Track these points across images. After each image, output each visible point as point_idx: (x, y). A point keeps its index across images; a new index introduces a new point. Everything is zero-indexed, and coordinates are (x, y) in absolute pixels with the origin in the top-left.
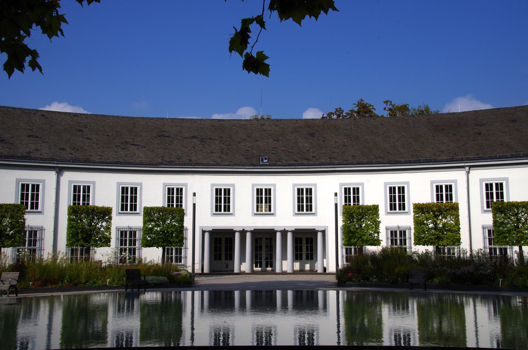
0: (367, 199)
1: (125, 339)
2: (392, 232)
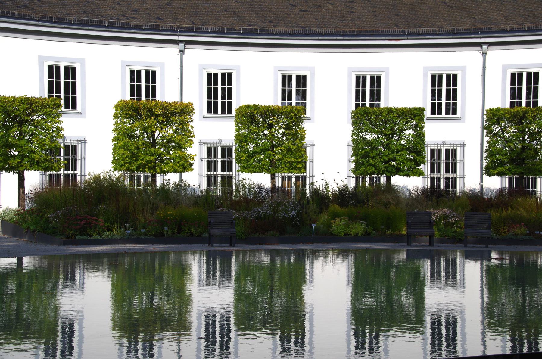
0: (393, 98)
1: (451, 331)
2: (209, 149)
